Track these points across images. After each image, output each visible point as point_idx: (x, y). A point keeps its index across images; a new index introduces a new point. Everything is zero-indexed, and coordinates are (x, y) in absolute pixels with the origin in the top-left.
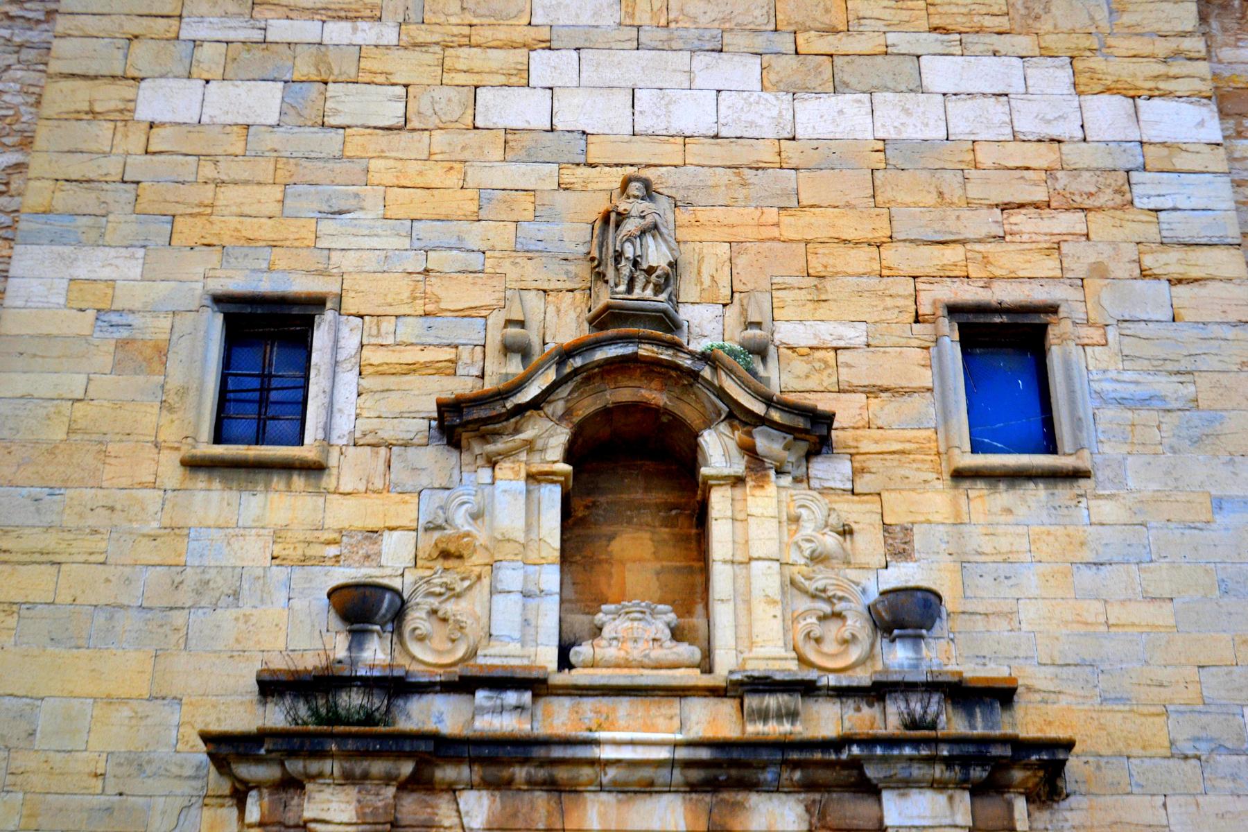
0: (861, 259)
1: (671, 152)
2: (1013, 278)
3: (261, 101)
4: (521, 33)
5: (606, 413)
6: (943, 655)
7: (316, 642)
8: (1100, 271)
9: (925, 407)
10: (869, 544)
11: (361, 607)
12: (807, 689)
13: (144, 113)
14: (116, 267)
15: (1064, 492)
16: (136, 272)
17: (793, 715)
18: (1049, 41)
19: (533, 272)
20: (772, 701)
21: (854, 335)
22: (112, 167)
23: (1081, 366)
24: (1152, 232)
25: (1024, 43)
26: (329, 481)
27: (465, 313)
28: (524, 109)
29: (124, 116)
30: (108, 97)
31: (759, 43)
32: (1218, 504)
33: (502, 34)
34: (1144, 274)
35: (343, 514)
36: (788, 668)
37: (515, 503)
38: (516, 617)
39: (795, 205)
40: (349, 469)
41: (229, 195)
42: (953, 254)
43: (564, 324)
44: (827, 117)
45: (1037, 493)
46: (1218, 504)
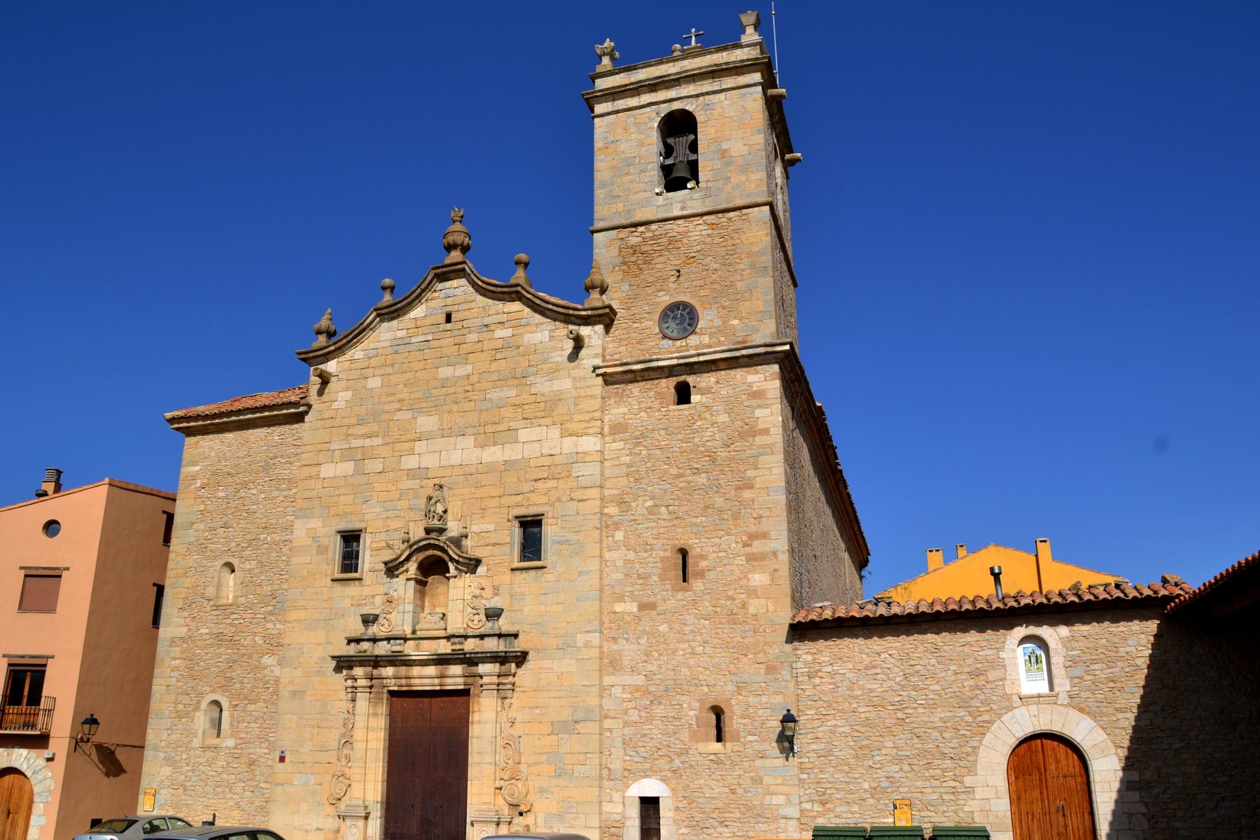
0: (494, 502)
1: (448, 472)
2: (535, 505)
3: (348, 468)
4: (413, 436)
5: (430, 557)
6: (504, 624)
7: (357, 628)
8: (559, 500)
9: (507, 548)
10: (488, 593)
11: (368, 620)
12: (466, 637)
13: (322, 476)
14: (316, 524)
15: (540, 572)
16: (320, 524)
17: (461, 643)
18: (555, 419)
19: (413, 515)
20: (456, 640)
21: (491, 527)
22: (315, 493)
23: (550, 532)
24: (575, 485)
25: (548, 421)
26: (363, 582)
27: (396, 530)
28: (411, 462)
29: (317, 477)
30: (313, 471)
31: (475, 431)
32: (580, 573)
33: (408, 437)
34: (571, 499)
35: (367, 591)
36: (462, 632)
37: (403, 587)
38: (400, 621)
39: (478, 486)
40: (367, 581)
41: (342, 499)
42: (519, 498)
43: (417, 533)
44: (494, 454)
45: (533, 573)
46: (580, 573)
